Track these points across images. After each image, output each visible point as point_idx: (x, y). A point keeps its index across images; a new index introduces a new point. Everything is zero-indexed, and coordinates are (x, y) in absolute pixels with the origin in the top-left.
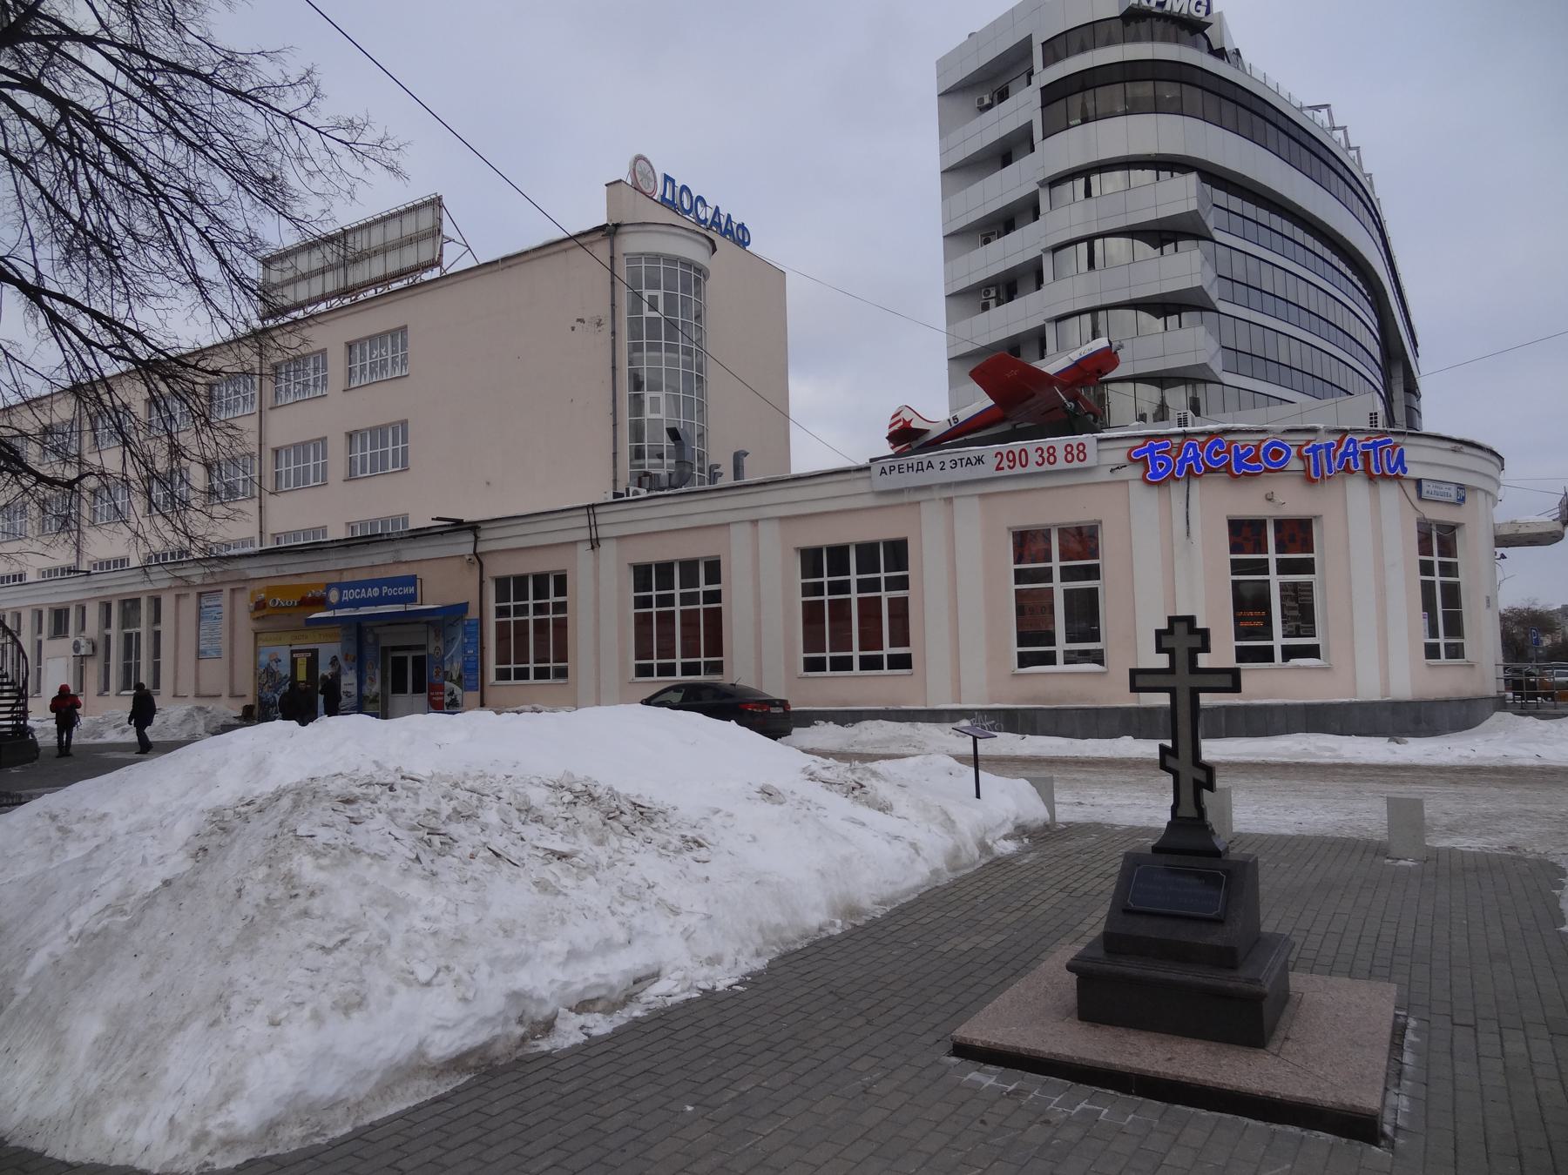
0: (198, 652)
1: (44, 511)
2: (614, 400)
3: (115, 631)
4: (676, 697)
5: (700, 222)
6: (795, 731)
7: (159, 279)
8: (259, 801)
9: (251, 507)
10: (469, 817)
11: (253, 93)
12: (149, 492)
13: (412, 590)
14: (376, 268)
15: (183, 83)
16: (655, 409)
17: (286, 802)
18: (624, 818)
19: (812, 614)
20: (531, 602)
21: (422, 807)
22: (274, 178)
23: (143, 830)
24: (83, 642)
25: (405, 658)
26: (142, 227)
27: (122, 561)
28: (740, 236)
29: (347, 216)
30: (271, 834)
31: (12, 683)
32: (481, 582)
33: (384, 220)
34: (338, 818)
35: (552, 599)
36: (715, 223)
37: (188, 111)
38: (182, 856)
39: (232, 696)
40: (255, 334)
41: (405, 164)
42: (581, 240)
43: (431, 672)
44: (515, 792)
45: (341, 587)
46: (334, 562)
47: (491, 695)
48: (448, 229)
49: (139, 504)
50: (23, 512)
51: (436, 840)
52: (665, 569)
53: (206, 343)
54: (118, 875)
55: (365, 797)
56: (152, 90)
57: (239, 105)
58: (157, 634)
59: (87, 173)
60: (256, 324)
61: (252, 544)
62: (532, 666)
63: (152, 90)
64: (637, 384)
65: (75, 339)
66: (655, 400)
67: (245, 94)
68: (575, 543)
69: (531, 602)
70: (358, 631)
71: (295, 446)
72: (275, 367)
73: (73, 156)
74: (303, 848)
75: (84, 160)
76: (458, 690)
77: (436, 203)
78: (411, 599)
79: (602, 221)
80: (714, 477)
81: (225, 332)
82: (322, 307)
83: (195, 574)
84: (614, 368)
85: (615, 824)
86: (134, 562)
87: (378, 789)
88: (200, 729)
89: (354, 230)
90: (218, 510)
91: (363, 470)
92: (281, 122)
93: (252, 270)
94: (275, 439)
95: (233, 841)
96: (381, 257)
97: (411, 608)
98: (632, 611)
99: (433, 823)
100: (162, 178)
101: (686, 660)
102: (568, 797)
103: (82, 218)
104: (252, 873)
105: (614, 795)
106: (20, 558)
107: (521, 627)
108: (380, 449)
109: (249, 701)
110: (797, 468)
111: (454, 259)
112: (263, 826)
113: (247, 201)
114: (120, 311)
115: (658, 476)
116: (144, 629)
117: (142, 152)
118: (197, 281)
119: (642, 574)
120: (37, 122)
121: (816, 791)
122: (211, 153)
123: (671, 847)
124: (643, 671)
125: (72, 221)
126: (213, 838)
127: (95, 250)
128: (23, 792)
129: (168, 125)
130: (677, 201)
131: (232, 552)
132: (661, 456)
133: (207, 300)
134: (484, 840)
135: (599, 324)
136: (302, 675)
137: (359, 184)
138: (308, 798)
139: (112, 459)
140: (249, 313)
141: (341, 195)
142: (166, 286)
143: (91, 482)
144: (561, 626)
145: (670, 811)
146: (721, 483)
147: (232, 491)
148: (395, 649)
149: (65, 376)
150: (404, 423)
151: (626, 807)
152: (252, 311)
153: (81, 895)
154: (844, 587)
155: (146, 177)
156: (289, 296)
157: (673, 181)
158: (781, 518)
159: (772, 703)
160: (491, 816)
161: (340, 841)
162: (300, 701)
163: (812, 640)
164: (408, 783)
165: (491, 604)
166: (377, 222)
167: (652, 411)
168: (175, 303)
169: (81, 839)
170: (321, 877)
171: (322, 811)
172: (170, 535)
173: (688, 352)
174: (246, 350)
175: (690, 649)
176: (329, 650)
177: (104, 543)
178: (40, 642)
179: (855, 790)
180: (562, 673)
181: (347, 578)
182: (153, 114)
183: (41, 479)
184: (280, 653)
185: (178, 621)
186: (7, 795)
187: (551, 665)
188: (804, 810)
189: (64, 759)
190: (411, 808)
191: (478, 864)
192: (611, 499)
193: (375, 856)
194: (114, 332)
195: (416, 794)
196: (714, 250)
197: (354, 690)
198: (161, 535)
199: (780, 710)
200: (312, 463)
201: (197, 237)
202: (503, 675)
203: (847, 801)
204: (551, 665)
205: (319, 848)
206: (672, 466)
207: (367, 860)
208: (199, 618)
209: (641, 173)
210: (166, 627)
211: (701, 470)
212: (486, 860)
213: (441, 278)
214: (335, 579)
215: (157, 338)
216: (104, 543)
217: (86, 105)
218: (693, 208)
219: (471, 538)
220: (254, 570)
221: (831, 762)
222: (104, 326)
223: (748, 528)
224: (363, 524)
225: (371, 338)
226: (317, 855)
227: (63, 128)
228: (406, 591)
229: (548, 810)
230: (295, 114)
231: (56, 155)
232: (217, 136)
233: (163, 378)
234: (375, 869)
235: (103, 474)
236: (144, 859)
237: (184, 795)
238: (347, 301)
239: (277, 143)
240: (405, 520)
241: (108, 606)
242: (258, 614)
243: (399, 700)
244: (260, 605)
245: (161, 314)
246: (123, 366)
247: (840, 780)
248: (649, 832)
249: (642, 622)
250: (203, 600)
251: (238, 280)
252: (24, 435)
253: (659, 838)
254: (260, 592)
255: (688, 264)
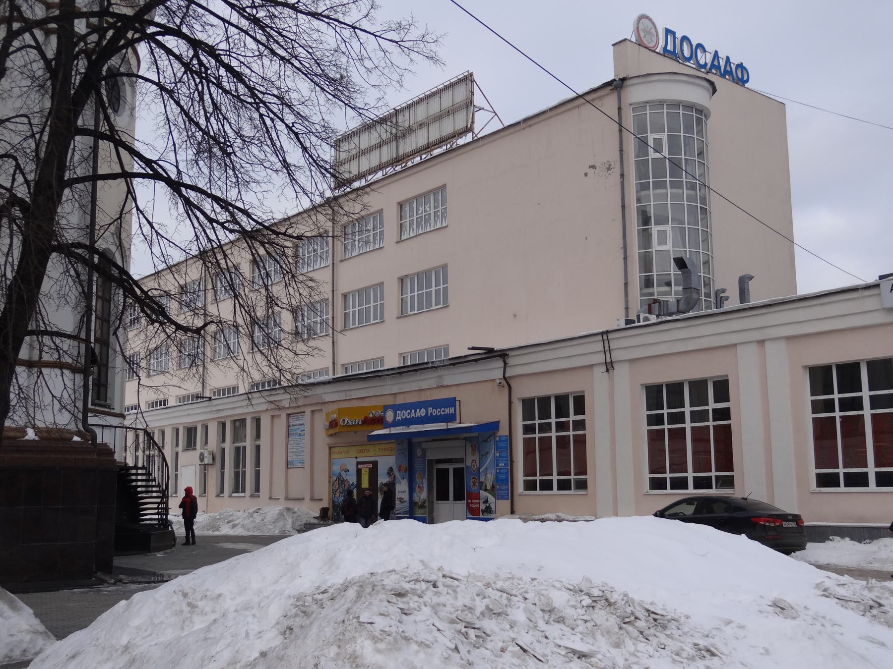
0: (287, 462)
1: (180, 352)
2: (624, 236)
3: (228, 445)
4: (689, 510)
5: (700, 67)
6: (809, 545)
7: (258, 168)
8: (331, 591)
9: (325, 344)
10: (499, 614)
11: (326, 13)
12: (252, 336)
13: (452, 410)
14: (421, 139)
15: (276, 13)
16: (662, 240)
17: (352, 593)
18: (639, 624)
19: (823, 431)
20: (553, 420)
21: (460, 603)
22: (342, 77)
23: (246, 609)
24: (206, 454)
25: (448, 470)
26: (248, 131)
27: (234, 388)
28: (738, 75)
29: (396, 99)
30: (340, 619)
31: (159, 486)
32: (510, 403)
33: (427, 98)
34: (392, 609)
35: (572, 417)
36: (715, 66)
37: (280, 34)
38: (274, 632)
39: (313, 499)
40: (328, 202)
41: (441, 52)
42: (588, 98)
43: (468, 481)
44: (539, 594)
45: (396, 408)
46: (390, 387)
47: (519, 503)
48: (478, 100)
49: (245, 344)
50: (167, 353)
51: (472, 633)
52: (675, 389)
53: (291, 213)
54: (229, 645)
55: (414, 592)
56: (255, 21)
57: (316, 23)
58: (258, 448)
59: (210, 94)
60: (328, 194)
61: (327, 374)
62: (555, 478)
63: (255, 21)
64: (645, 220)
65: (202, 218)
66: (662, 234)
67: (320, 14)
68: (591, 366)
69: (553, 420)
70: (409, 445)
71: (359, 291)
72: (345, 227)
73: (201, 78)
74: (364, 633)
75: (209, 81)
76: (491, 499)
77: (468, 79)
78: (451, 418)
79: (609, 76)
80: (720, 300)
81: (306, 204)
82: (379, 175)
83: (284, 399)
84: (623, 206)
85: (629, 628)
86: (242, 391)
87: (424, 586)
88: (289, 527)
89: (403, 109)
90: (301, 347)
91: (412, 309)
92: (347, 32)
93: (327, 153)
94: (344, 287)
95: (312, 623)
96: (424, 130)
97: (451, 426)
98: (645, 428)
99: (469, 617)
100: (262, 89)
101: (697, 472)
102: (587, 601)
103: (207, 126)
104: (326, 651)
105: (629, 602)
106: (165, 390)
107: (545, 443)
108: (426, 289)
109: (325, 504)
110: (803, 289)
111: (484, 124)
112: (334, 612)
113: (322, 97)
114: (232, 195)
115: (667, 302)
116: (249, 443)
117: (248, 72)
118: (286, 165)
119: (654, 394)
120: (179, 58)
121: (830, 607)
122: (297, 63)
123: (684, 655)
124: (657, 484)
125: (201, 129)
126: (297, 619)
127: (215, 150)
128: (164, 572)
129: (267, 47)
130: (678, 51)
131: (312, 380)
132: (669, 284)
133: (293, 180)
134: (513, 635)
135: (609, 169)
136: (365, 484)
137: (407, 75)
138: (368, 590)
139: (225, 309)
140: (325, 188)
141: (391, 85)
142: (263, 174)
143: (212, 328)
144: (581, 441)
145: (683, 619)
146: (727, 306)
147: (311, 333)
148: (439, 461)
149: (195, 247)
150: (445, 267)
151: (641, 614)
152: (325, 186)
153: (203, 660)
154: (857, 404)
155: (251, 90)
156: (354, 168)
157: (674, 33)
158: (788, 338)
159: (785, 517)
160: (519, 614)
161: (394, 629)
162: (359, 505)
163: (825, 455)
164: (449, 581)
165: (519, 423)
166: (421, 100)
167: (660, 244)
168: (269, 187)
169: (203, 613)
170: (379, 659)
171: (379, 602)
172: (266, 369)
173: (692, 187)
174: (321, 217)
175: (701, 464)
176: (387, 462)
177: (221, 375)
178: (177, 453)
179: (872, 608)
180: (582, 485)
181: (400, 400)
182: (255, 39)
183: (179, 327)
184: (348, 464)
185: (273, 435)
186: (155, 574)
187: (572, 477)
188: (818, 627)
189: (191, 547)
190: (452, 603)
191: (507, 657)
192: (623, 326)
193: (421, 644)
194: (227, 210)
195: (455, 591)
196: (714, 90)
197: (406, 496)
198: (259, 368)
199: (793, 525)
200: (372, 305)
201: (286, 131)
202: (530, 486)
203: (864, 620)
204: (572, 477)
205: (377, 633)
206: (681, 292)
207: (414, 647)
208: (288, 435)
209: (645, 30)
210: (264, 442)
211: (708, 295)
212: (514, 655)
213: (473, 142)
214: (390, 401)
215: (258, 214)
216: (221, 375)
217: (210, 42)
218: (693, 54)
219: (501, 364)
220: (329, 394)
221: (846, 578)
222: (222, 207)
223: (754, 348)
224: (412, 354)
225: (417, 197)
226: (375, 639)
227: (195, 62)
228: (447, 411)
229: (569, 612)
230: (357, 25)
231: (191, 81)
232: (300, 50)
233: (262, 244)
234: (422, 655)
235: (220, 322)
236: (247, 633)
237: (276, 582)
238: (398, 168)
239: (344, 50)
240: (446, 349)
241: (224, 425)
242: (332, 431)
243: (441, 506)
244: (333, 424)
245: (260, 196)
246: (232, 237)
247: (855, 598)
248: (662, 638)
249: (655, 438)
250: (291, 420)
251: (316, 162)
252: (168, 294)
253: (672, 645)
254: (333, 413)
255: (689, 106)
